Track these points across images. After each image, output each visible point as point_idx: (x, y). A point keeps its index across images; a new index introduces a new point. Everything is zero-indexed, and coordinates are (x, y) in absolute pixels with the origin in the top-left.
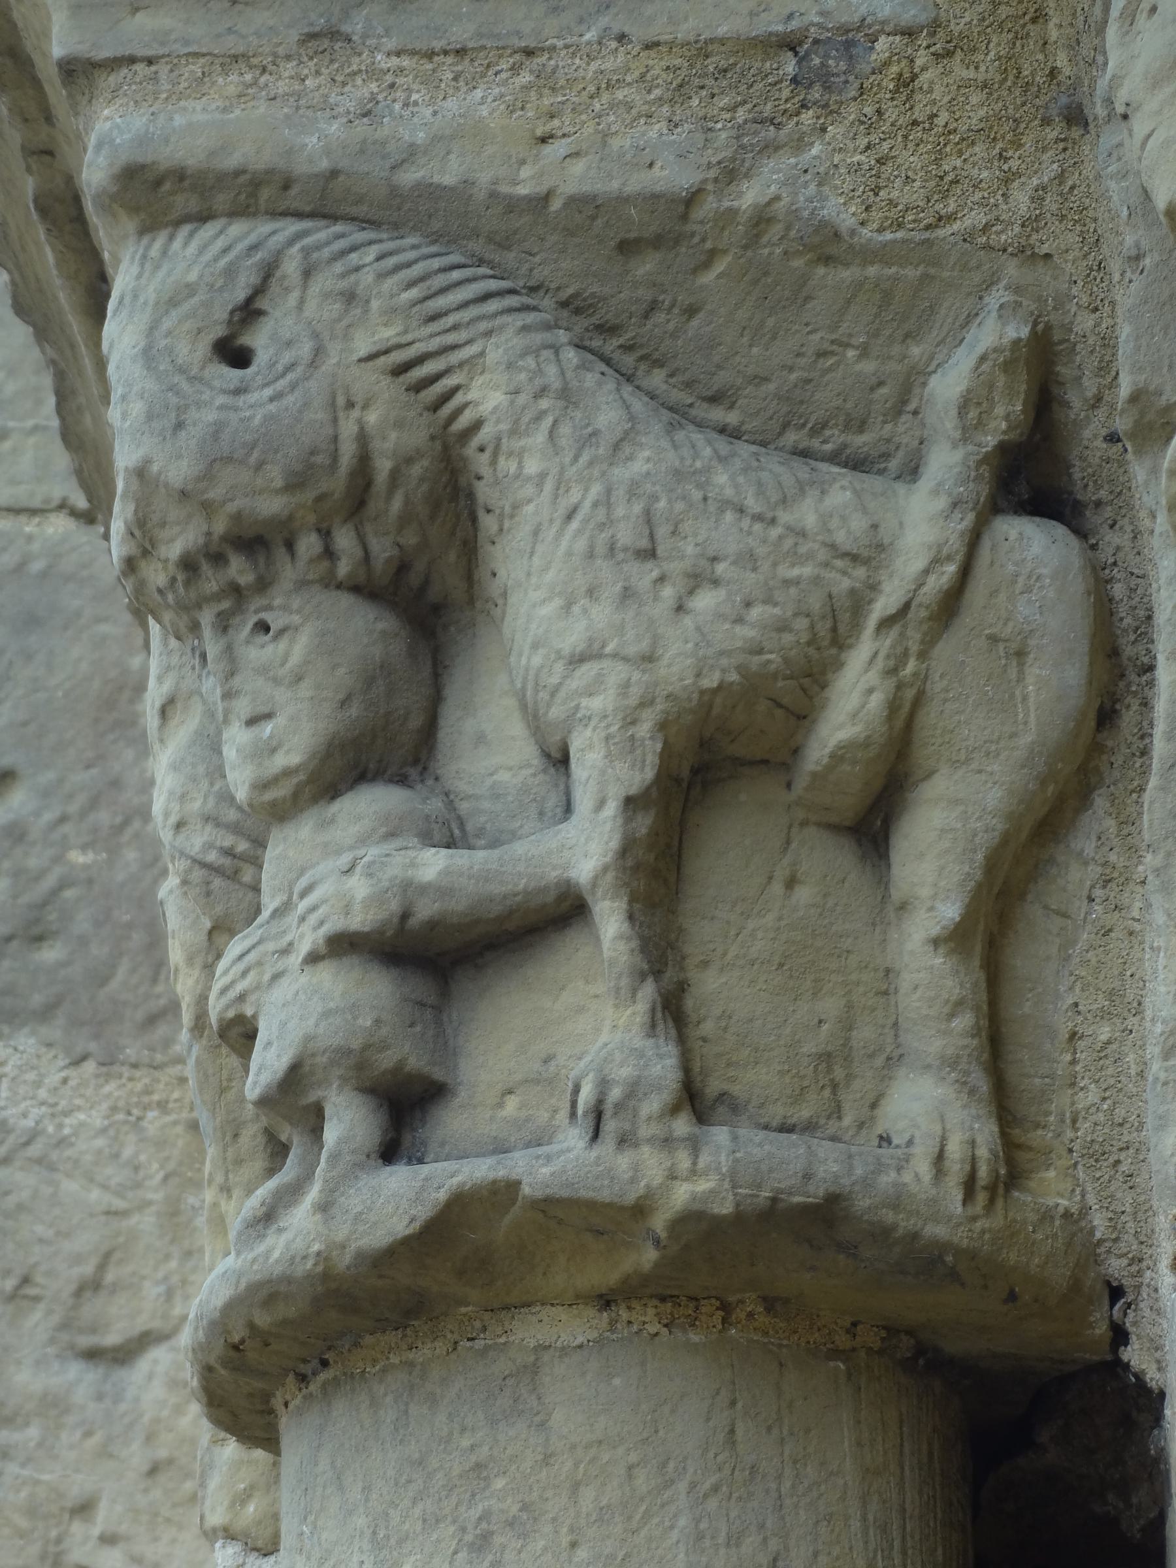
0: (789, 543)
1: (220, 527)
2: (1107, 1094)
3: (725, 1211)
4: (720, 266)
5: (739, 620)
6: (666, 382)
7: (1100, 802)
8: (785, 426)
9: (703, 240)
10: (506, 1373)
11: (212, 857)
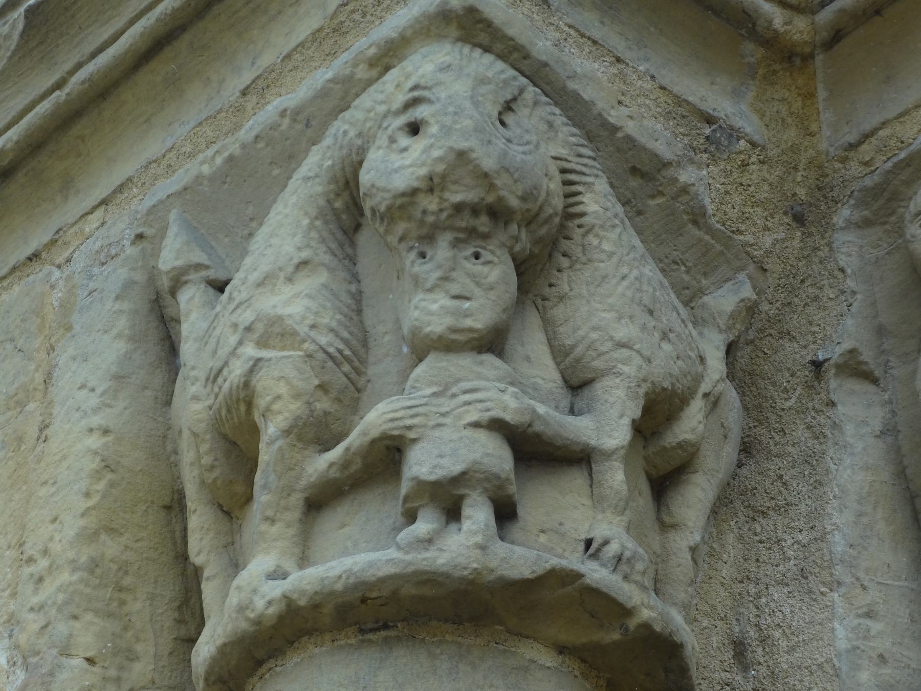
1: (490, 199)
3: (658, 630)
4: (660, 200)
9: (661, 185)
10: (514, 666)
11: (331, 350)
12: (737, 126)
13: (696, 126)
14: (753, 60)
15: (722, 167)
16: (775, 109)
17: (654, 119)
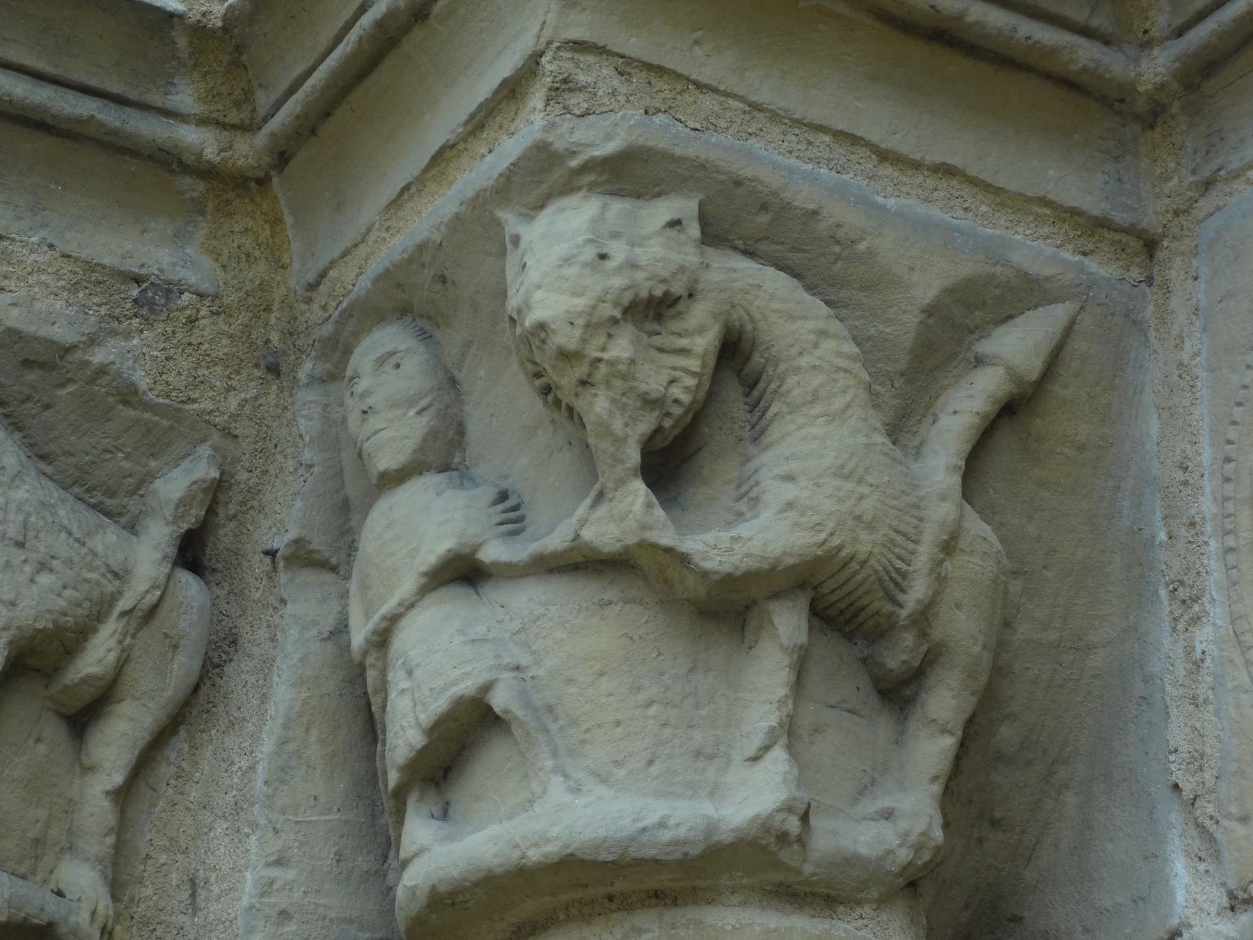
0: (89, 558)
2: (157, 892)
5: (59, 595)
6: (20, 440)
7: (183, 733)
8: (74, 483)
9: (67, 372)
12: (177, 278)
13: (118, 288)
14: (195, 194)
15: (159, 330)
16: (235, 245)
17: (52, 296)
